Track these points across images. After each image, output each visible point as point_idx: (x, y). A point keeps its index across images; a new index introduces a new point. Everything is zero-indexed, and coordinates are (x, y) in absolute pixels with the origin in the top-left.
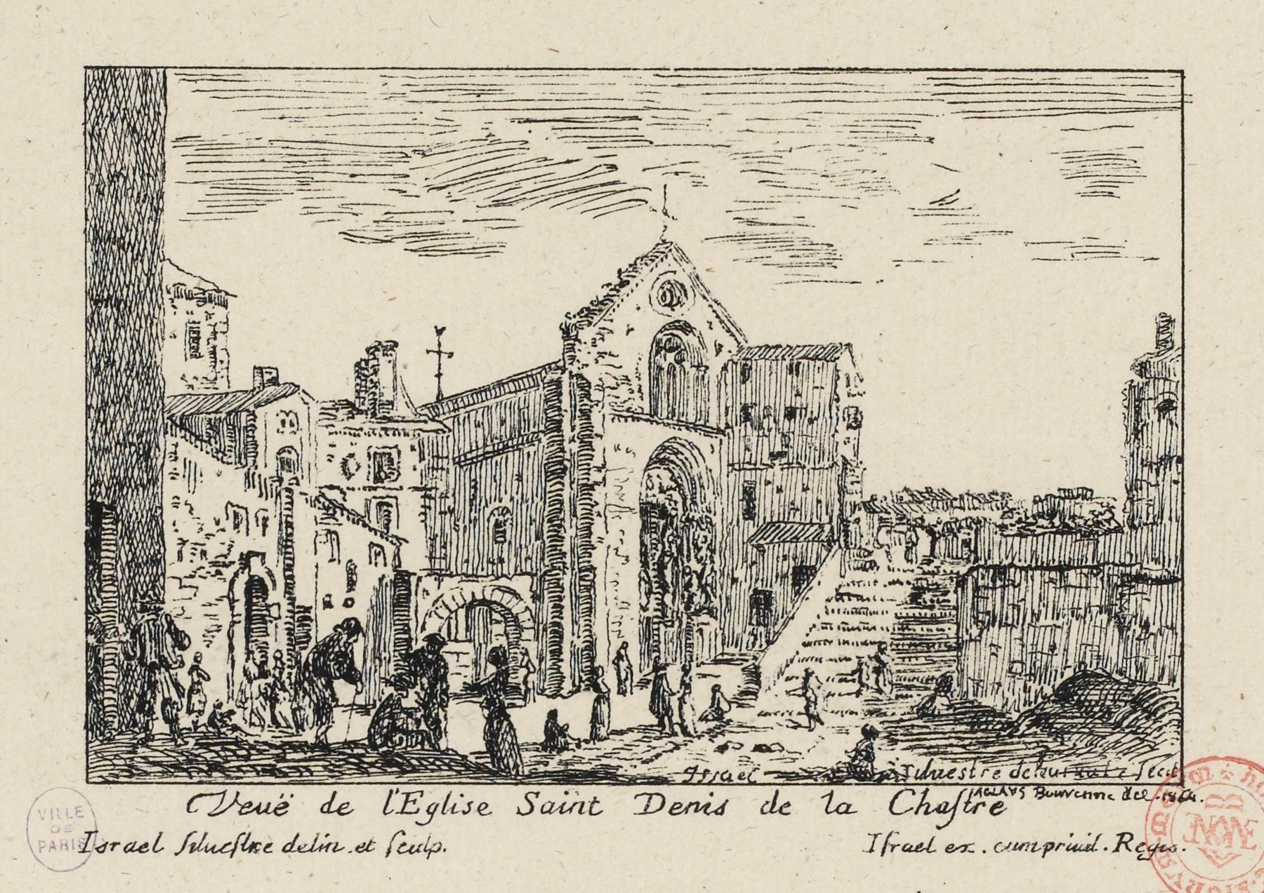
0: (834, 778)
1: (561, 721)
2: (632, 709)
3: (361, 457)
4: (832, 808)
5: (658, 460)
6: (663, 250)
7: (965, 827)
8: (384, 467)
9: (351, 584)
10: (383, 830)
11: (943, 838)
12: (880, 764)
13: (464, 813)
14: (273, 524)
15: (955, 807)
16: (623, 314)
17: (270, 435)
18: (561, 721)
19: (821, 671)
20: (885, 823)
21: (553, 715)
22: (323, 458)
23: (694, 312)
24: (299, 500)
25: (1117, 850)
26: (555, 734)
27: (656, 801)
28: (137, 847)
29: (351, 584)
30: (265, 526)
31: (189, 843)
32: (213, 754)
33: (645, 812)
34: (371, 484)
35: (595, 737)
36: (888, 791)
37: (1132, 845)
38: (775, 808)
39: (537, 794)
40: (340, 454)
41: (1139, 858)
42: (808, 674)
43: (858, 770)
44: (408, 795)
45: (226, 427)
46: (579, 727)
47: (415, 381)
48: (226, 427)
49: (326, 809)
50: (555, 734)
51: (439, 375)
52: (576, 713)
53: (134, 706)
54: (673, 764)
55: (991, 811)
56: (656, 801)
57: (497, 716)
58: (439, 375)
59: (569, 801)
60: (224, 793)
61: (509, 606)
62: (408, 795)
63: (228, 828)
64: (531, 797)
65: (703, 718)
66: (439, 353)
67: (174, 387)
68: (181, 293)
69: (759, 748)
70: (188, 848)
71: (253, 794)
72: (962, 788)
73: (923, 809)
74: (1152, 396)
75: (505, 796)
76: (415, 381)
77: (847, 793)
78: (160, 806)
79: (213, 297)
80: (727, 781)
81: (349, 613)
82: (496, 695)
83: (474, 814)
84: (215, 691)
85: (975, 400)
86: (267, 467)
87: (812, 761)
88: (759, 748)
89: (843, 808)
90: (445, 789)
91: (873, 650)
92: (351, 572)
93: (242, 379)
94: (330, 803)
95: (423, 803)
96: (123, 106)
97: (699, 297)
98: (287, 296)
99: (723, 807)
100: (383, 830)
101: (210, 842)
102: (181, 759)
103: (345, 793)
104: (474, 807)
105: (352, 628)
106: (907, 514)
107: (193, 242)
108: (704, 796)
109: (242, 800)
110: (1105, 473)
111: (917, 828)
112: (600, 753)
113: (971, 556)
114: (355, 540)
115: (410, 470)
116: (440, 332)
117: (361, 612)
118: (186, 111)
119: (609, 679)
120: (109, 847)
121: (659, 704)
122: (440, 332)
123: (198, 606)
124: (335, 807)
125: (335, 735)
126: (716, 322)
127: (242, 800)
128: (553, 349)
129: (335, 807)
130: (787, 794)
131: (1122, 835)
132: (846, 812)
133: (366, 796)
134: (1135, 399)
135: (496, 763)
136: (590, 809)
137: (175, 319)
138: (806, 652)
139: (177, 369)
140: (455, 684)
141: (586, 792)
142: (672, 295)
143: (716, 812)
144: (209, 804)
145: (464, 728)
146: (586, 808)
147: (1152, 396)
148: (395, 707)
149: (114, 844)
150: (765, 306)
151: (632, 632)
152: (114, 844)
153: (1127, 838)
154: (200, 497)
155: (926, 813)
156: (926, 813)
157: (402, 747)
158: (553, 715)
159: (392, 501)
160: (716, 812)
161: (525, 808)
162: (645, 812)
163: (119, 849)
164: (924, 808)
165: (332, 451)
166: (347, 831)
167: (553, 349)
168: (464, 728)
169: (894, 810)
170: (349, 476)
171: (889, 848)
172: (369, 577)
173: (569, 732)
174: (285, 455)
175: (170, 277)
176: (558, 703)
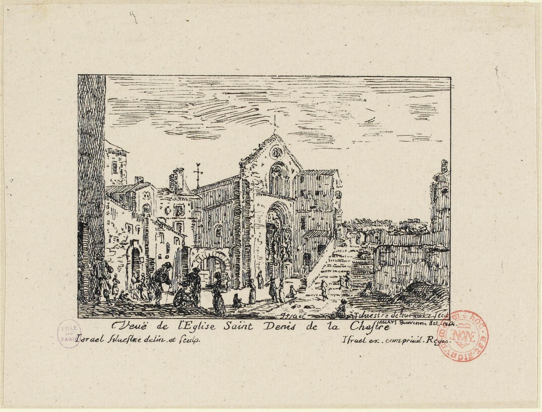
0: (332, 317)
1: (239, 298)
2: (263, 294)
6: (274, 137)
7: (376, 334)
8: (179, 211)
9: (168, 251)
10: (178, 334)
11: (368, 338)
12: (347, 313)
14: (141, 230)
15: (373, 327)
16: (260, 159)
17: (141, 201)
18: (239, 298)
19: (327, 281)
20: (349, 333)
21: (236, 295)
23: (285, 158)
24: (150, 222)
25: (428, 342)
26: (237, 302)
27: (271, 325)
29: (168, 251)
30: (139, 231)
32: (121, 308)
33: (267, 329)
34: (175, 217)
35: (250, 303)
36: (350, 322)
38: (311, 327)
39: (231, 322)
40: (164, 206)
42: (323, 282)
43: (340, 315)
44: (187, 322)
45: (126, 197)
46: (245, 300)
47: (190, 182)
48: (126, 197)
49: (159, 327)
50: (237, 302)
51: (198, 180)
52: (244, 295)
53: (93, 292)
54: (277, 312)
56: (271, 325)
57: (217, 296)
58: (198, 180)
59: (242, 324)
62: (187, 322)
63: (126, 333)
64: (229, 323)
66: (198, 172)
67: (108, 183)
68: (110, 151)
69: (306, 307)
70: (112, 340)
71: (134, 322)
72: (375, 321)
73: (362, 328)
74: (440, 188)
75: (219, 323)
76: (190, 182)
77: (336, 322)
78: (103, 326)
79: (121, 153)
80: (295, 318)
81: (167, 261)
82: (217, 289)
83: (209, 329)
84: (121, 287)
85: (380, 189)
86: (140, 211)
87: (324, 312)
88: (306, 307)
89: (335, 328)
90: (199, 321)
92: (168, 247)
93: (131, 181)
94: (160, 325)
95: (192, 325)
96: (91, 88)
98: (147, 153)
99: (294, 327)
100: (178, 334)
103: (165, 322)
104: (209, 327)
105: (168, 266)
106: (357, 227)
107: (114, 134)
108: (287, 323)
109: (131, 324)
110: (425, 217)
111: (360, 334)
113: (378, 242)
114: (169, 236)
115: (188, 212)
116: (198, 165)
117: (171, 260)
118: (112, 90)
119: (255, 283)
121: (272, 292)
122: (198, 165)
123: (116, 258)
124: (162, 326)
125: (162, 302)
126: (292, 162)
127: (131, 324)
128: (237, 171)
129: (162, 326)
130: (315, 322)
131: (429, 337)
132: (336, 329)
133: (173, 323)
134: (434, 189)
135: (217, 312)
136: (249, 327)
137: (108, 160)
139: (109, 177)
140: (203, 285)
141: (247, 322)
142: (277, 153)
143: (291, 329)
147: (440, 188)
148: (181, 293)
149: (87, 339)
150: (311, 157)
151: (263, 267)
152: (87, 339)
154: (117, 221)
155: (363, 329)
158: (236, 295)
159: (182, 223)
160: (291, 329)
161: (227, 327)
162: (267, 329)
164: (362, 328)
165: (162, 205)
166: (166, 335)
167: (237, 171)
168: (206, 300)
170: (167, 214)
171: (350, 341)
172: (174, 248)
173: (242, 301)
174: (146, 207)
175: (107, 146)
176: (238, 291)
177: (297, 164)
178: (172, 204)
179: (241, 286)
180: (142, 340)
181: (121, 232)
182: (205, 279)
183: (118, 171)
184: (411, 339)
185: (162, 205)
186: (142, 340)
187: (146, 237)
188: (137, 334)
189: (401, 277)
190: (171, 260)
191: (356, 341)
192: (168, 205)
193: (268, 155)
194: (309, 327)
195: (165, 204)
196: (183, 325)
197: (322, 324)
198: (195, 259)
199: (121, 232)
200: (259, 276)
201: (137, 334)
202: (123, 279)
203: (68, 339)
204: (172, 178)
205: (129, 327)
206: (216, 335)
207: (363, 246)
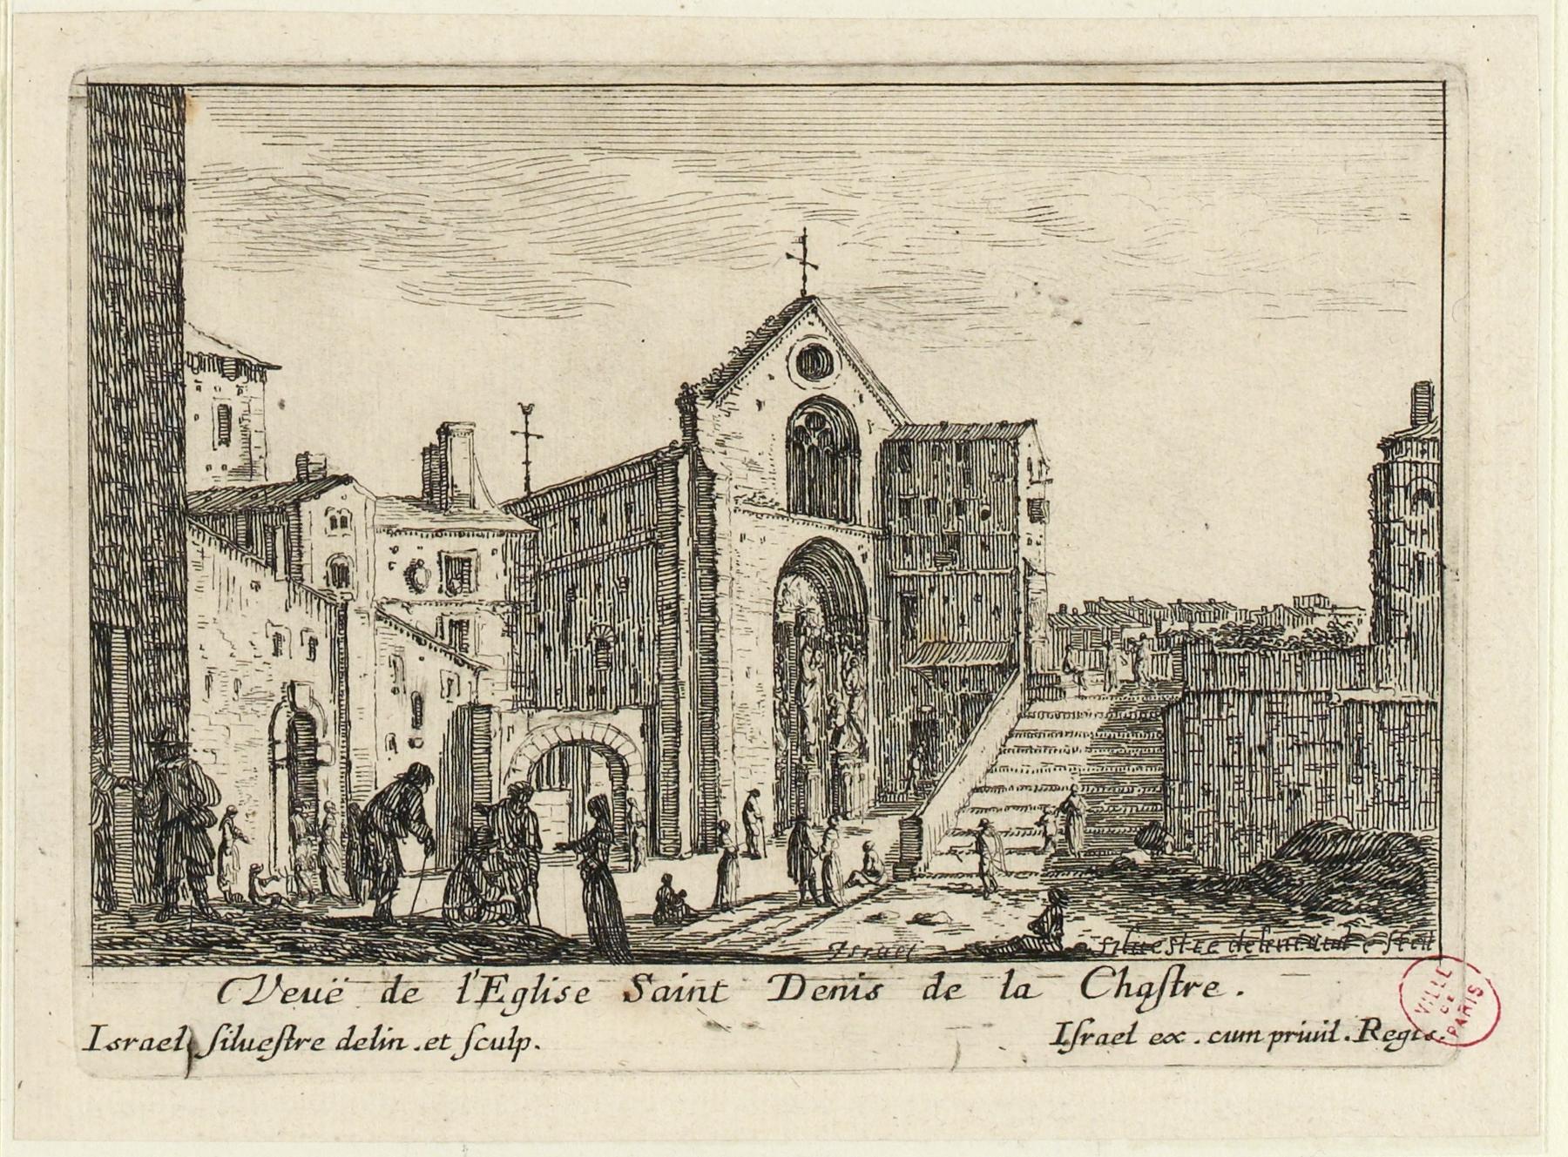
0: (1016, 950)
2: (766, 874)
3: (431, 562)
4: (1010, 991)
5: (796, 564)
6: (806, 303)
7: (1172, 1013)
8: (458, 570)
9: (417, 723)
10: (459, 1022)
11: (1151, 1024)
13: (557, 1001)
15: (1162, 989)
16: (754, 382)
17: (319, 546)
19: (999, 822)
20: (1078, 1009)
21: (667, 880)
22: (382, 565)
23: (841, 385)
24: (353, 620)
25: (1361, 1039)
26: (670, 904)
28: (155, 1044)
29: (417, 723)
30: (312, 651)
31: (220, 1038)
33: (781, 997)
35: (720, 907)
38: (936, 991)
39: (649, 978)
40: (403, 562)
41: (1387, 1049)
43: (1042, 945)
44: (491, 979)
45: (263, 520)
46: (700, 895)
47: (494, 473)
48: (263, 520)
50: (670, 904)
52: (696, 879)
53: (159, 876)
54: (822, 937)
56: (795, 986)
57: (597, 878)
58: (527, 463)
59: (687, 984)
60: (264, 976)
62: (491, 979)
63: (264, 1021)
71: (296, 977)
74: (1407, 476)
76: (494, 473)
78: (181, 994)
79: (249, 369)
80: (881, 956)
82: (595, 859)
85: (1180, 494)
86: (316, 575)
92: (418, 702)
93: (282, 471)
96: (136, 133)
97: (763, 462)
98: (339, 359)
100: (459, 1022)
102: (927, 556)
105: (416, 777)
106: (1098, 623)
107: (222, 303)
110: (1352, 587)
111: (1113, 1014)
112: (727, 926)
116: (527, 411)
117: (430, 756)
118: (207, 140)
119: (736, 837)
120: (122, 1045)
122: (527, 411)
123: (229, 749)
128: (668, 431)
129: (399, 995)
131: (1367, 1021)
133: (438, 982)
134: (1382, 482)
135: (607, 941)
139: (206, 468)
141: (703, 974)
142: (813, 361)
145: (560, 902)
146: (708, 994)
147: (1407, 476)
150: (922, 381)
151: (766, 778)
153: (1373, 1024)
154: (233, 617)
155: (1127, 995)
156: (1127, 995)
157: (490, 935)
158: (667, 880)
160: (868, 997)
163: (134, 1046)
164: (1123, 989)
165: (394, 558)
166: (409, 1023)
167: (668, 431)
169: (1089, 992)
170: (415, 587)
175: (193, 344)
177: (883, 395)
178: (429, 551)
181: (248, 654)
187: (341, 671)
188: (310, 1019)
189: (1266, 811)
190: (430, 756)
191: (1104, 1040)
192: (418, 555)
193: (780, 372)
194: (931, 992)
196: (476, 988)
197: (981, 979)
199: (248, 654)
200: (748, 807)
201: (310, 1019)
202: (259, 842)
203: (1461, 1016)
204: (436, 455)
205: (279, 994)
206: (588, 1018)
207: (1114, 691)
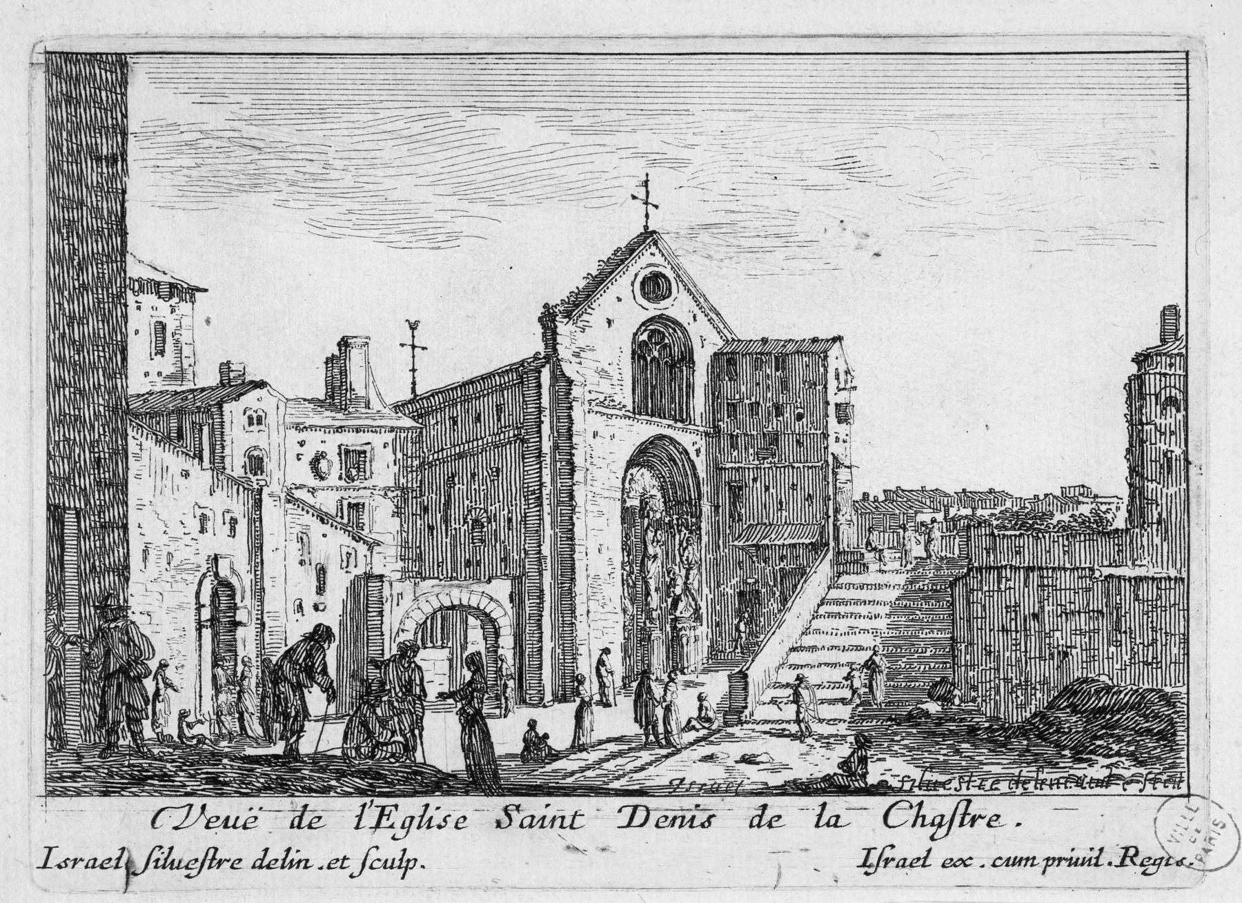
1: (541, 731)
2: (616, 720)
3: (332, 454)
4: (824, 820)
6: (648, 237)
7: (960, 841)
8: (355, 461)
9: (321, 590)
10: (356, 845)
11: (942, 851)
12: (875, 774)
14: (242, 527)
16: (605, 303)
18: (541, 731)
19: (813, 676)
21: (532, 725)
22: (291, 456)
23: (679, 307)
24: (267, 502)
26: (535, 745)
29: (321, 590)
30: (233, 529)
35: (578, 747)
36: (879, 804)
37: (1138, 860)
39: (518, 807)
40: (309, 453)
41: (1144, 873)
42: (800, 679)
43: (849, 782)
44: (383, 808)
45: (191, 419)
46: (560, 739)
47: (386, 379)
48: (191, 419)
50: (535, 745)
51: (413, 370)
52: (557, 724)
53: (104, 719)
54: (663, 774)
55: (989, 825)
56: (641, 815)
57: (473, 722)
58: (413, 370)
59: (550, 813)
61: (487, 611)
62: (383, 808)
63: (191, 844)
65: (689, 727)
66: (413, 347)
68: (144, 286)
70: (152, 865)
72: (959, 799)
73: (920, 820)
76: (386, 379)
77: (837, 804)
85: (967, 398)
86: (236, 464)
89: (833, 821)
91: (863, 656)
92: (322, 572)
96: (87, 93)
100: (356, 845)
101: (897, 854)
105: (320, 636)
106: (894, 510)
108: (692, 809)
110: (1111, 479)
111: (911, 841)
112: (583, 764)
113: (986, 542)
114: (330, 544)
115: (383, 470)
117: (331, 618)
119: (590, 688)
120: (70, 864)
123: (163, 612)
128: (531, 344)
130: (777, 804)
131: (1127, 849)
132: (835, 825)
133: (339, 810)
134: (1136, 390)
137: (143, 313)
138: (795, 658)
140: (432, 692)
141: (564, 805)
142: (654, 287)
143: (702, 825)
144: (178, 817)
145: (442, 743)
146: (567, 822)
147: (1156, 385)
150: (749, 302)
151: (616, 638)
154: (167, 499)
155: (923, 825)
157: (383, 771)
158: (532, 725)
159: (367, 448)
160: (702, 825)
163: (81, 865)
165: (301, 450)
166: (310, 845)
167: (531, 344)
168: (442, 743)
169: (890, 822)
172: (338, 583)
175: (135, 270)
179: (548, 697)
180: (247, 863)
182: (435, 668)
183: (169, 346)
184: (1068, 855)
185: (301, 450)
186: (247, 863)
188: (230, 843)
191: (903, 863)
195: (315, 443)
196: (371, 816)
197: (797, 812)
198: (402, 614)
200: (601, 663)
201: (230, 843)
204: (337, 363)
205: (203, 821)
